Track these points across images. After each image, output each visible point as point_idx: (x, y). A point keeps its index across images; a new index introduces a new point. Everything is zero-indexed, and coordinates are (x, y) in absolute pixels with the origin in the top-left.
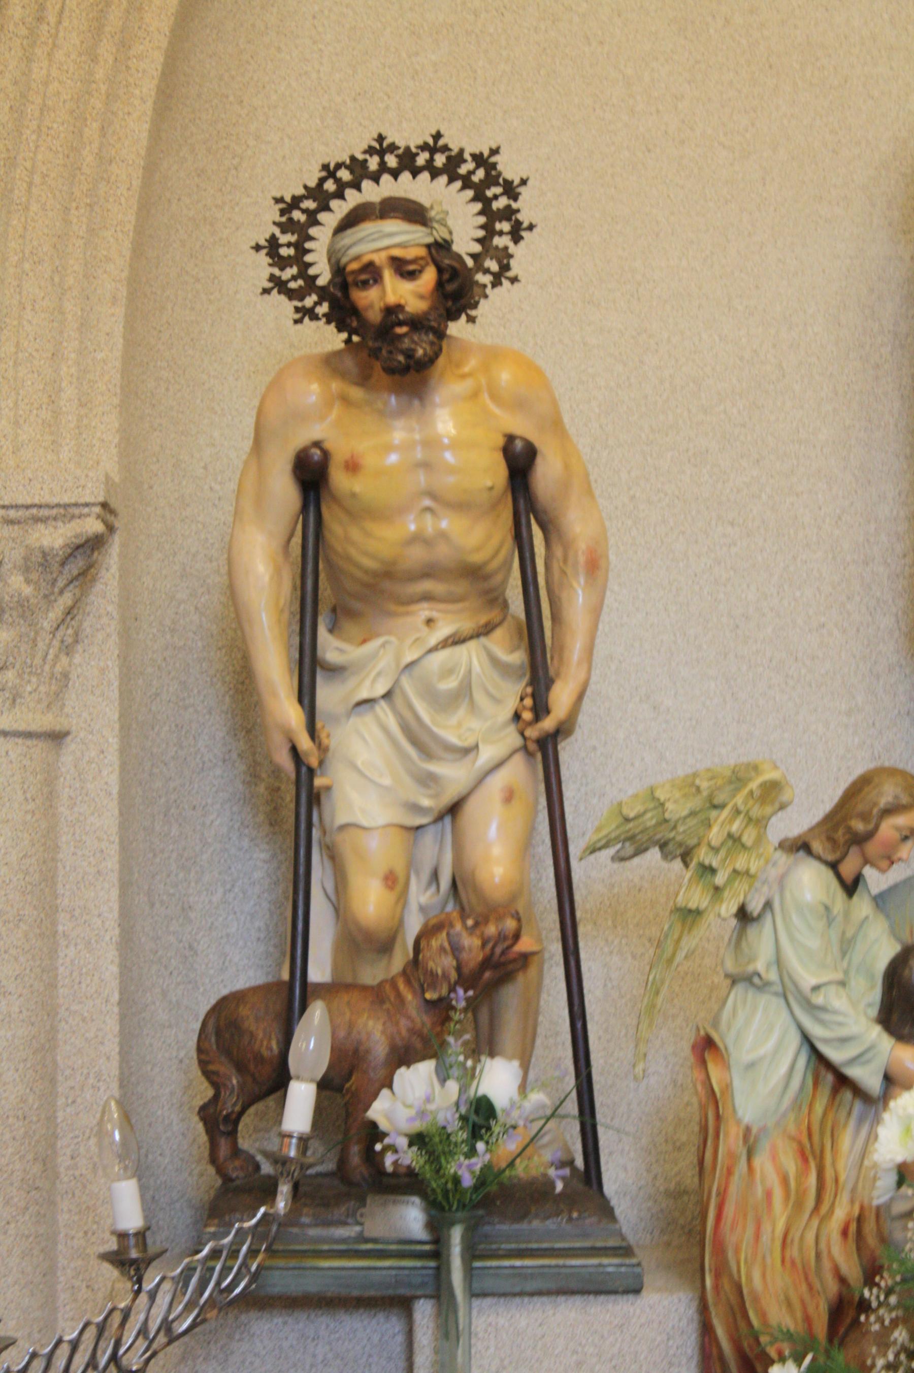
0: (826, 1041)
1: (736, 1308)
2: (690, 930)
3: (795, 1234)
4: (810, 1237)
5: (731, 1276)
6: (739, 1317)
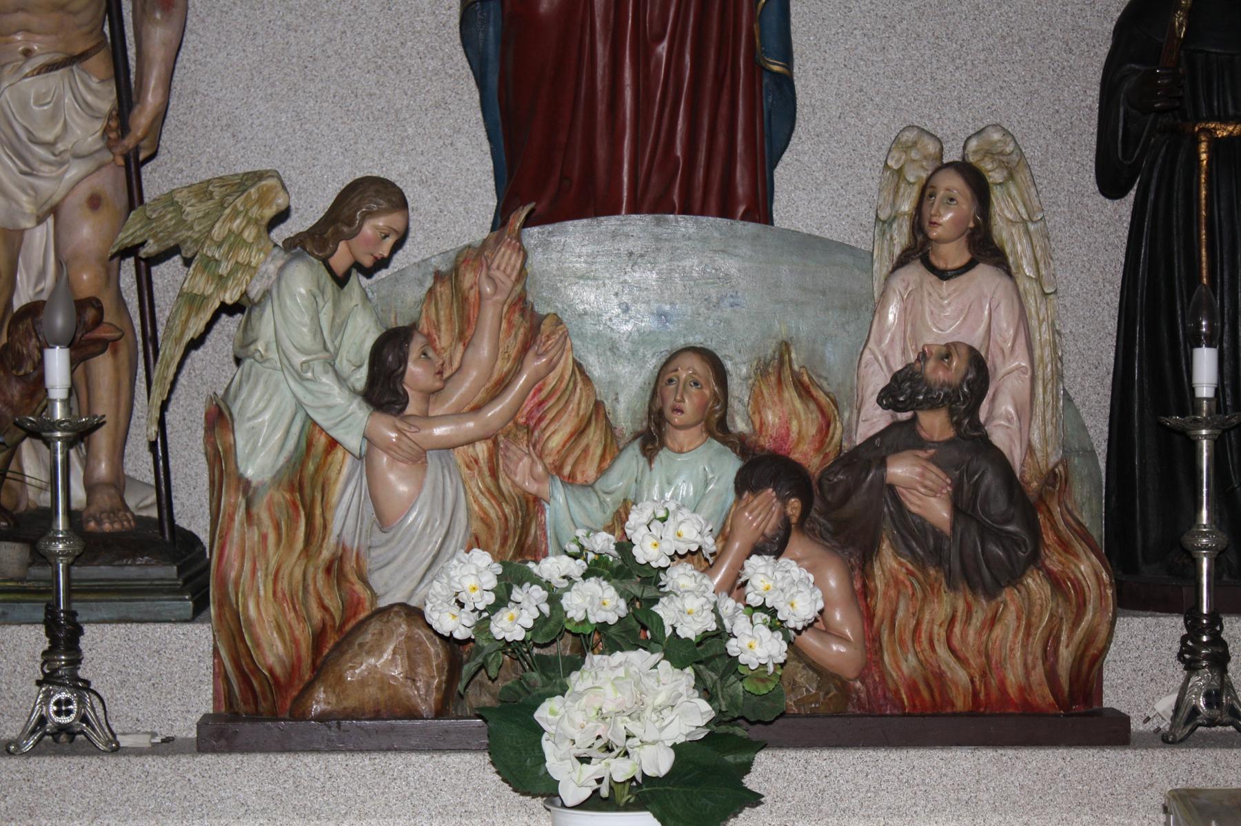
0: (314, 408)
1: (235, 633)
2: (197, 314)
3: (285, 572)
4: (298, 573)
5: (231, 604)
6: (238, 641)
